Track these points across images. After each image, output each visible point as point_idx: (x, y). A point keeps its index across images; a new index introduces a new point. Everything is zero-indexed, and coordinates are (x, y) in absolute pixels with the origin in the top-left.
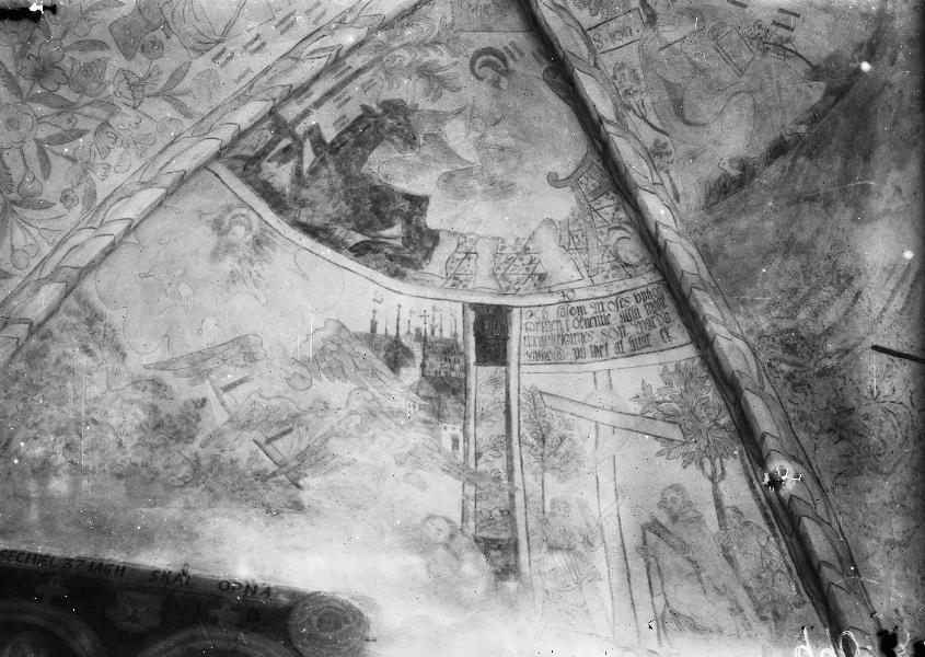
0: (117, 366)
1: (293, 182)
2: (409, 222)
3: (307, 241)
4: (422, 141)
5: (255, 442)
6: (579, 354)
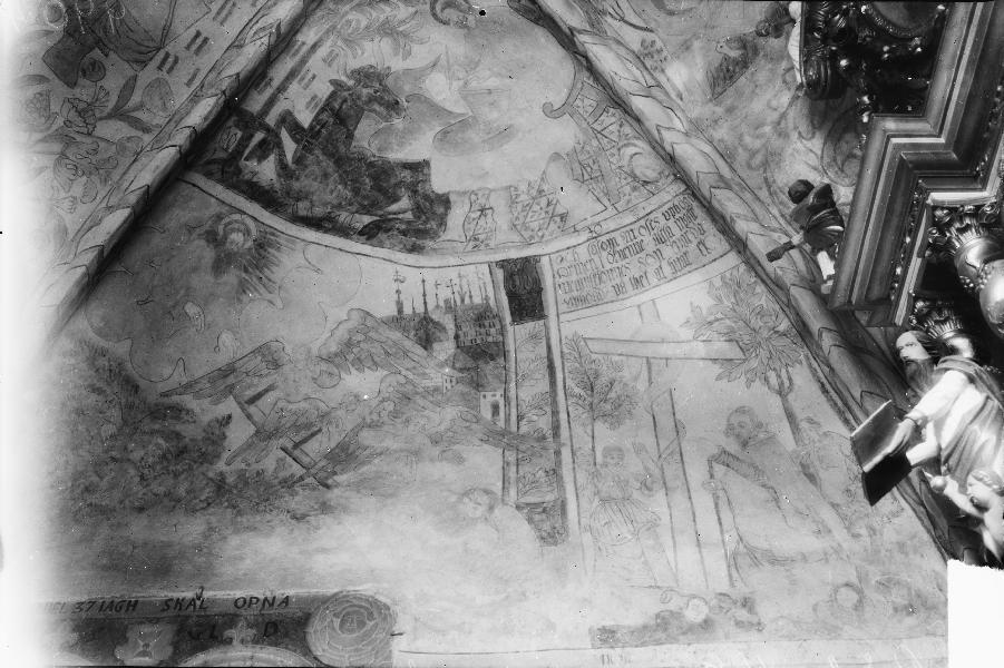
0: (130, 399)
1: (279, 175)
3: (311, 235)
5: (282, 449)
6: (619, 289)
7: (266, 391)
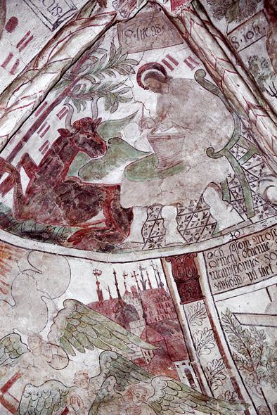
2: (109, 207)
3: (31, 243)
4: (108, 144)
7: (14, 379)
